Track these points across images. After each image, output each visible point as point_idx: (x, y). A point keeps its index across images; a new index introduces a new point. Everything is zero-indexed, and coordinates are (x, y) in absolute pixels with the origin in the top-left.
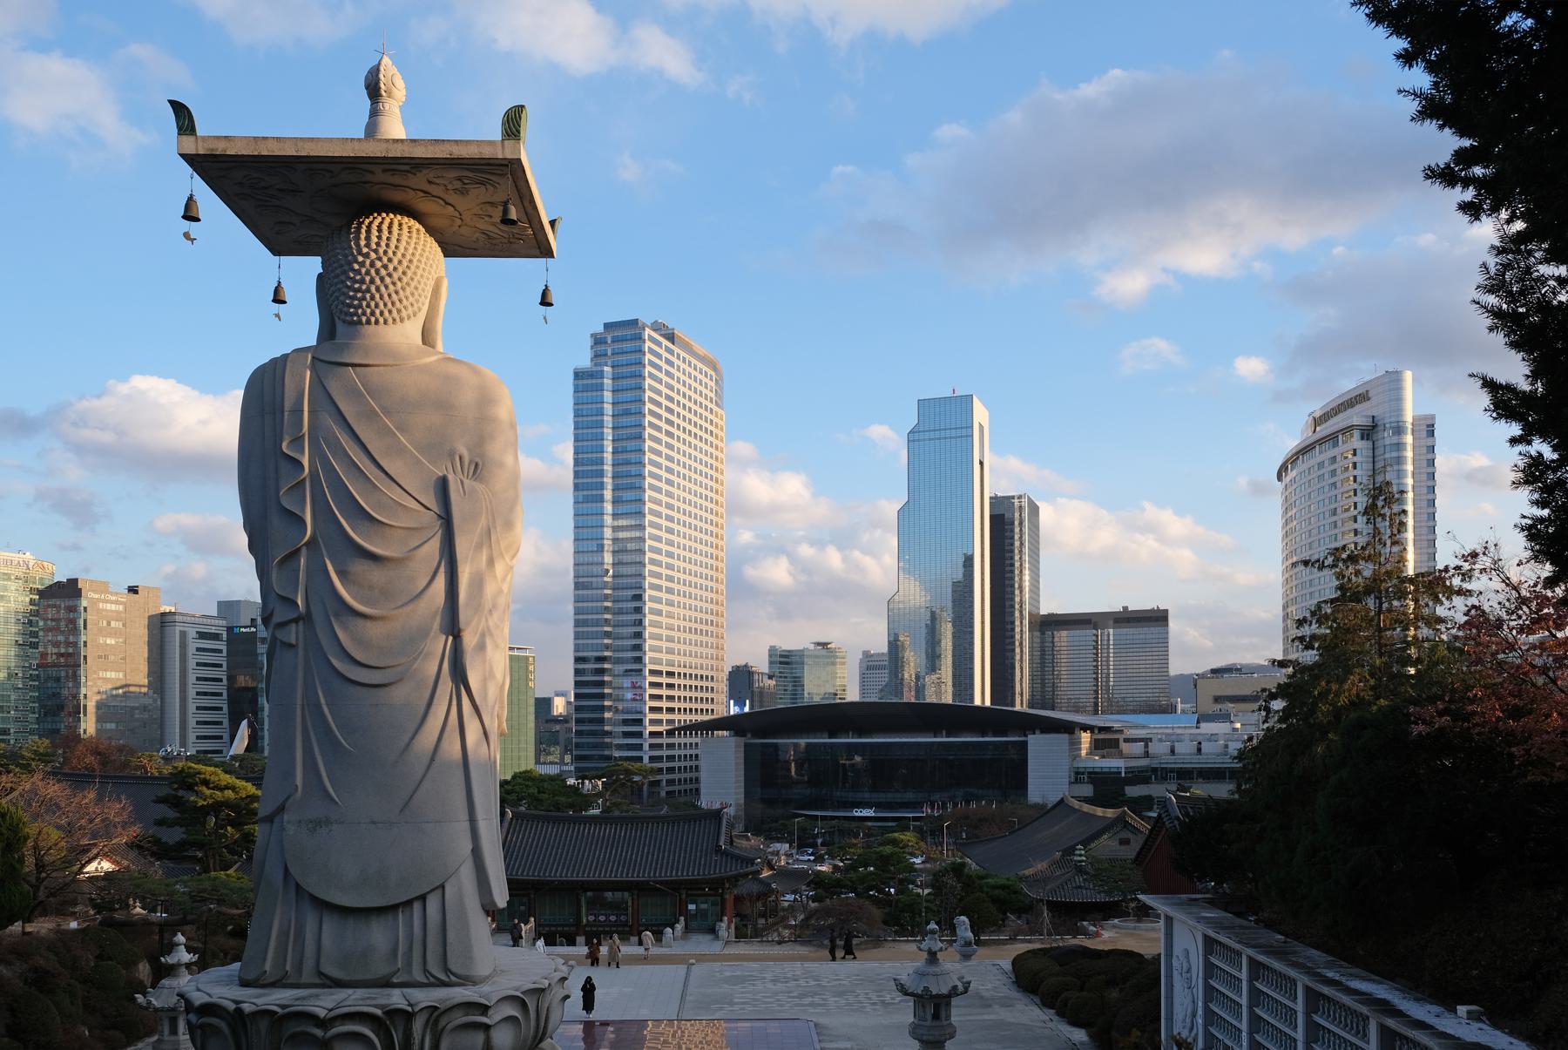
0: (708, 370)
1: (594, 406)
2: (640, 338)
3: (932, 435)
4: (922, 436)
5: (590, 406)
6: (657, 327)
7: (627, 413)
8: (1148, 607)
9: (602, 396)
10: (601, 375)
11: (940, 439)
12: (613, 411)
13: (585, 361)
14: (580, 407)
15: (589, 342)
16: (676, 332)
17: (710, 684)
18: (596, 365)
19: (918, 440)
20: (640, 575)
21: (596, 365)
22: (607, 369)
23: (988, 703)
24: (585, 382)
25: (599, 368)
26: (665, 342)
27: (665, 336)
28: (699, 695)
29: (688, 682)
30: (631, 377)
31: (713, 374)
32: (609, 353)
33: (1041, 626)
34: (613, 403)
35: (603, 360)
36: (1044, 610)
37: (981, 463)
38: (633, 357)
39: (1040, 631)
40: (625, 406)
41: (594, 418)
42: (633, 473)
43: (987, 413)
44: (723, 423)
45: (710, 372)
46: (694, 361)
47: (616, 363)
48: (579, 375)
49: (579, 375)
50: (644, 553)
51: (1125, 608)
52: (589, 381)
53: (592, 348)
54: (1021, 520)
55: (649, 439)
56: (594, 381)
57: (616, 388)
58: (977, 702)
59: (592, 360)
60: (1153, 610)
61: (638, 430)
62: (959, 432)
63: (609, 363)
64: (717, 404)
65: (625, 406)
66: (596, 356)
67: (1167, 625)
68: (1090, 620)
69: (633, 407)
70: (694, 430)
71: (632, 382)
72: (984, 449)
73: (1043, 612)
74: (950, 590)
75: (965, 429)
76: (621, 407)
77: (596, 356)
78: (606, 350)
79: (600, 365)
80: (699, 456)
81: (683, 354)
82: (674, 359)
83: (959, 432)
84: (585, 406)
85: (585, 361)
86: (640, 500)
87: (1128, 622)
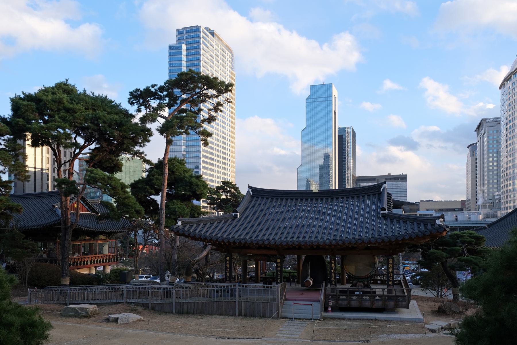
0: (228, 53)
1: (178, 62)
2: (199, 31)
3: (316, 100)
4: (311, 100)
5: (176, 62)
6: (207, 29)
7: (193, 65)
8: (399, 174)
9: (182, 58)
10: (181, 48)
11: (319, 101)
12: (187, 65)
13: (174, 42)
14: (172, 62)
15: (175, 33)
16: (214, 32)
17: (229, 153)
18: (179, 43)
19: (310, 102)
20: (198, 162)
21: (179, 43)
22: (184, 47)
23: (337, 188)
24: (174, 51)
25: (180, 45)
26: (210, 35)
27: (210, 33)
28: (224, 161)
29: (222, 150)
30: (195, 49)
31: (231, 55)
32: (185, 38)
33: (356, 181)
34: (186, 61)
35: (182, 41)
36: (357, 175)
37: (335, 112)
38: (195, 39)
39: (356, 183)
40: (192, 63)
41: (178, 68)
42: (195, 65)
43: (337, 92)
44: (235, 78)
45: (229, 54)
46: (222, 47)
47: (188, 43)
48: (171, 48)
49: (171, 48)
50: (200, 152)
51: (389, 174)
52: (176, 51)
53: (177, 36)
54: (349, 139)
55: (203, 157)
56: (178, 51)
57: (188, 66)
58: (334, 188)
59: (177, 42)
60: (401, 175)
61: (197, 39)
62: (326, 99)
63: (185, 43)
64: (232, 69)
65: (192, 63)
66: (179, 40)
67: (406, 181)
68: (376, 179)
69: (195, 62)
70: (222, 150)
71: (195, 51)
72: (337, 105)
73: (357, 175)
74: (318, 169)
75: (330, 97)
76: (190, 63)
77: (179, 40)
78: (183, 37)
79: (181, 43)
80: (222, 145)
81: (217, 43)
82: (214, 65)
83: (326, 99)
84: (174, 62)
85: (174, 42)
86: (199, 151)
87: (391, 180)
